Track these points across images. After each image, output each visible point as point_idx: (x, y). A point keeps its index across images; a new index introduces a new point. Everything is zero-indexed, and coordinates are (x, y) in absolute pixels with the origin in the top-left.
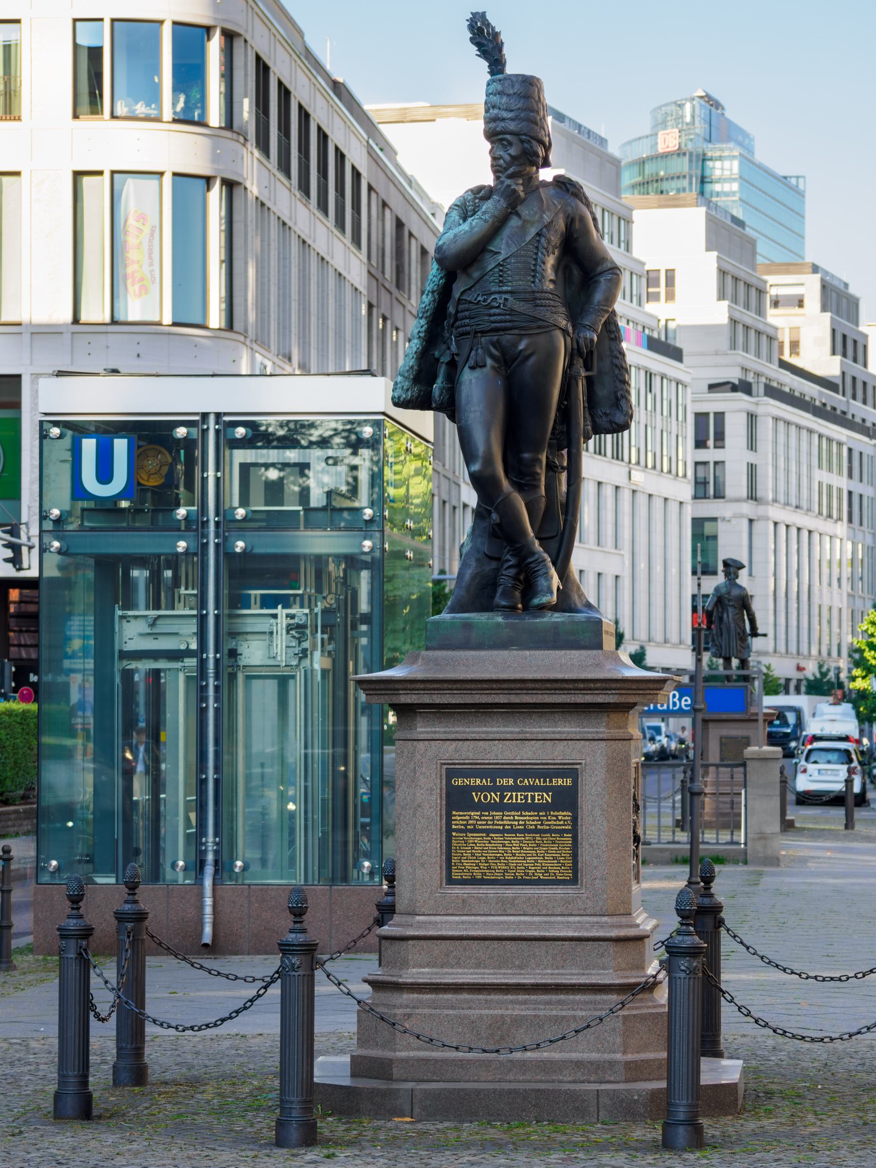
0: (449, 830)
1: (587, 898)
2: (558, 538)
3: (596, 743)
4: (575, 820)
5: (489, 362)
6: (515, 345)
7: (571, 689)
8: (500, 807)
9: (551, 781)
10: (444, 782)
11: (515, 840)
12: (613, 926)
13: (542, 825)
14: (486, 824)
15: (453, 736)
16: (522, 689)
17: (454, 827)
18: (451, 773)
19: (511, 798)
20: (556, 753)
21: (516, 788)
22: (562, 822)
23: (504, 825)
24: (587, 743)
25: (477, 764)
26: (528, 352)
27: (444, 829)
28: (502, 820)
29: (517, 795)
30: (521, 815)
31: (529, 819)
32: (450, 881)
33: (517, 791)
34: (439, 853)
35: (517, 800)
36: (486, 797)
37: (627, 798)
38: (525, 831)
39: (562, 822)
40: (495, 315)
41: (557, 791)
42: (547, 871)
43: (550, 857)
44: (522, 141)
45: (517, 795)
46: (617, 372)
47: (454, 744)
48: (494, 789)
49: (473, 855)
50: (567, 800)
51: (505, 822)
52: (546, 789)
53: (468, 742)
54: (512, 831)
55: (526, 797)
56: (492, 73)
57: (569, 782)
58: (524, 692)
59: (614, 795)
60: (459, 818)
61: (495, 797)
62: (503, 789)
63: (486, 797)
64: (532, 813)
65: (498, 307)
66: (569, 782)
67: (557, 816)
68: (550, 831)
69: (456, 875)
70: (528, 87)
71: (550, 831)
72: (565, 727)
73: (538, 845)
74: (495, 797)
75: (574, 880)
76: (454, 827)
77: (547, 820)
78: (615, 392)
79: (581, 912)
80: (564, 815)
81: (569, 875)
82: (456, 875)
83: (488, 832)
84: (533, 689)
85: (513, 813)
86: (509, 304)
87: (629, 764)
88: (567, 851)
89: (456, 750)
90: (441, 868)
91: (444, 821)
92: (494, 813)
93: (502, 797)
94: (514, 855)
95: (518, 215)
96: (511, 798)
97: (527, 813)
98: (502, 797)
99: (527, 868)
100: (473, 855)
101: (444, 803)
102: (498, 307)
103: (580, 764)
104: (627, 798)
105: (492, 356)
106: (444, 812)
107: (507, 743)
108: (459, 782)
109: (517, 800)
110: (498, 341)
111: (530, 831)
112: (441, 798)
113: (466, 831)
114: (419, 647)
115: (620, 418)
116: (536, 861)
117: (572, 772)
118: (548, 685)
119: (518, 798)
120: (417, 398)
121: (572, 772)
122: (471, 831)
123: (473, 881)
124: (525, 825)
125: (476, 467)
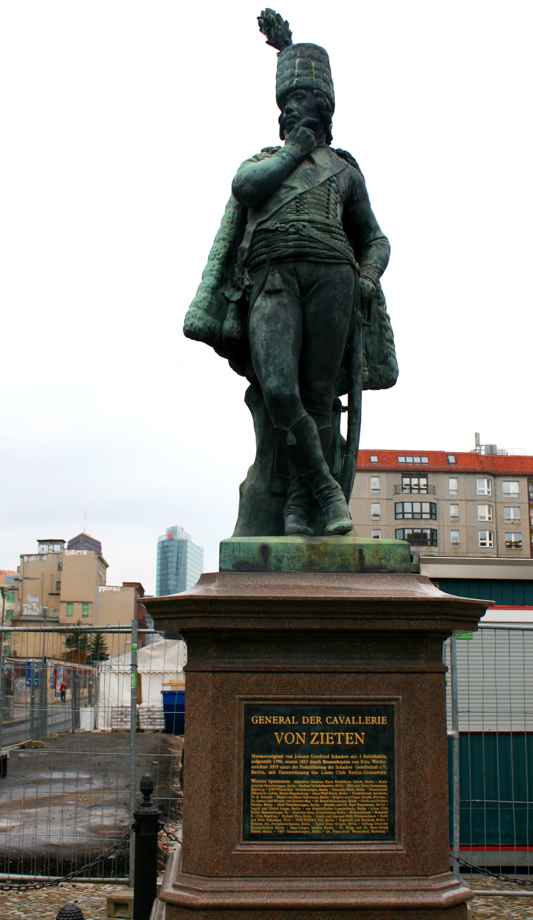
1: (407, 855)
9: (363, 720)
14: (291, 770)
17: (253, 772)
18: (251, 710)
19: (318, 738)
22: (376, 767)
23: (310, 771)
28: (309, 764)
29: (325, 736)
30: (330, 759)
31: (341, 762)
35: (325, 740)
39: (376, 767)
42: (359, 824)
45: (325, 736)
47: (255, 676)
49: (275, 805)
53: (270, 676)
55: (336, 738)
57: (383, 720)
60: (259, 761)
61: (300, 738)
62: (309, 728)
64: (342, 757)
66: (383, 720)
67: (370, 760)
74: (300, 738)
75: (390, 835)
77: (360, 765)
80: (378, 759)
81: (384, 828)
83: (292, 778)
84: (352, 613)
85: (321, 756)
93: (309, 738)
94: (322, 805)
96: (318, 738)
100: (275, 805)
103: (397, 700)
108: (259, 720)
109: (325, 740)
111: (340, 777)
124: (334, 770)
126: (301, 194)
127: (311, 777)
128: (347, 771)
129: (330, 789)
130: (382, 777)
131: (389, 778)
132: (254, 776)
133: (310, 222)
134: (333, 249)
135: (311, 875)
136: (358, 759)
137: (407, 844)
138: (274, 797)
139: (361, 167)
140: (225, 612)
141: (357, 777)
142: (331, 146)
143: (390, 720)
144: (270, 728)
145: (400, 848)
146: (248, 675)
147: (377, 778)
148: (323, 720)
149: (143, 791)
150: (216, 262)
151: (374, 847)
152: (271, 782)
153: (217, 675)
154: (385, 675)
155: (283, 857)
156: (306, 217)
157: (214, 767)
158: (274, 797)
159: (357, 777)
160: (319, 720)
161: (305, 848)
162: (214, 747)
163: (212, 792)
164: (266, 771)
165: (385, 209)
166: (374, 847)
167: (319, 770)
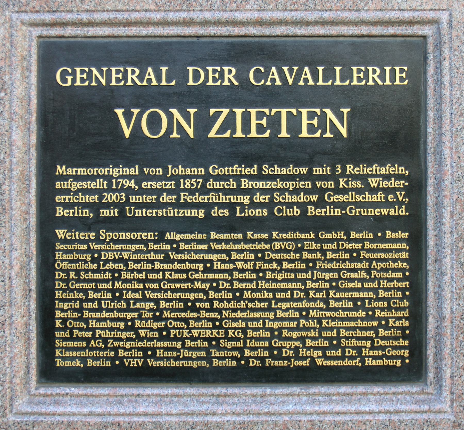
4: (416, 188)
8: (197, 151)
9: (347, 75)
11: (240, 249)
13: (320, 204)
14: (158, 205)
17: (60, 212)
18: (53, 54)
19: (230, 123)
22: (379, 197)
23: (208, 206)
28: (204, 191)
30: (260, 177)
31: (285, 189)
35: (393, 79)
36: (154, 122)
39: (379, 197)
41: (360, 101)
42: (335, 343)
48: (181, 97)
49: (117, 295)
51: (212, 197)
54: (231, 224)
55: (274, 122)
60: (79, 184)
61: (181, 122)
62: (204, 98)
63: (154, 122)
64: (292, 170)
66: (398, 76)
67: (364, 178)
73: (311, 266)
76: (60, 212)
77: (338, 191)
80: (386, 174)
83: (161, 226)
85: (235, 170)
88: (394, 281)
92: (181, 170)
93: (204, 124)
96: (230, 123)
97: (278, 170)
98: (204, 124)
99: (277, 334)
100: (117, 295)
108: (76, 77)
109: (393, 79)
111: (287, 224)
113: (96, 224)
116: (304, 313)
119: (249, 123)
124: (270, 205)
127: (209, 224)
128: (303, 206)
129: (259, 255)
136: (334, 177)
138: (116, 276)
143: (417, 75)
144: (108, 98)
147: (380, 224)
152: (105, 235)
167: (231, 206)
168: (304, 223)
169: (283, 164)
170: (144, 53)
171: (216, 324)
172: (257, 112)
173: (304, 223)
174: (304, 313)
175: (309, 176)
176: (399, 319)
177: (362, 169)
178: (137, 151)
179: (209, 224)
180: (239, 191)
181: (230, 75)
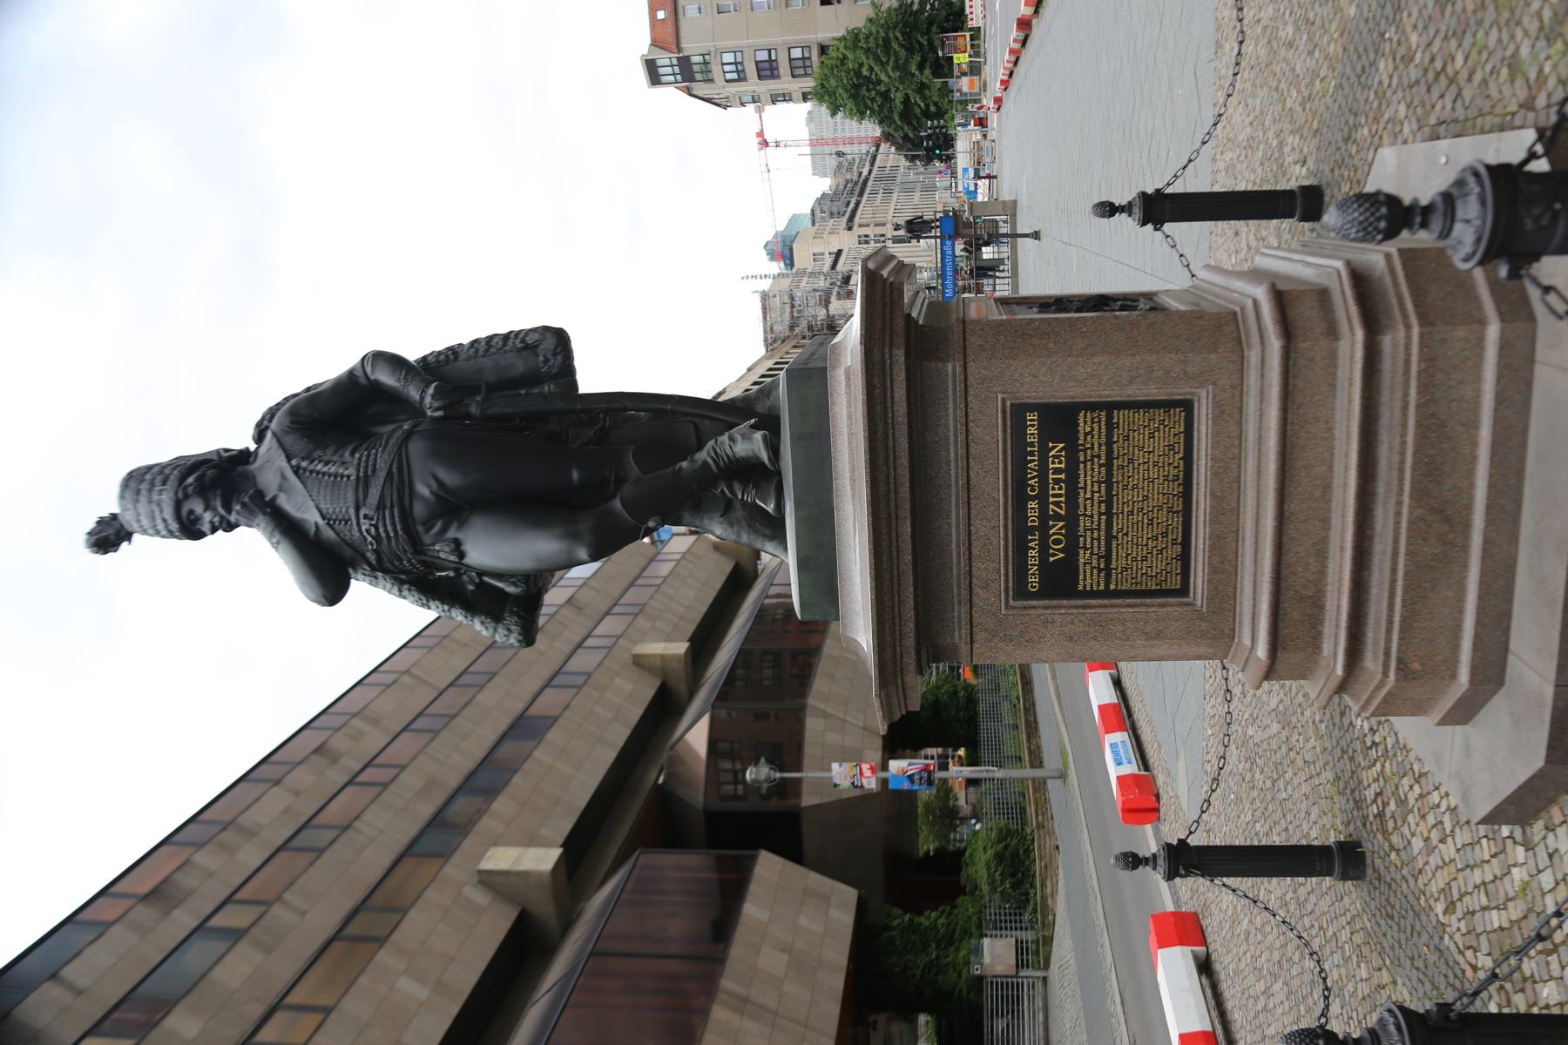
0: (1106, 594)
1: (1215, 384)
2: (697, 421)
3: (970, 378)
4: (1092, 407)
5: (451, 534)
6: (425, 500)
7: (886, 423)
8: (1071, 520)
9: (1032, 444)
10: (1034, 603)
11: (1123, 497)
12: (1394, 364)
13: (1099, 456)
14: (1099, 539)
15: (965, 593)
16: (889, 501)
17: (1102, 587)
18: (1021, 592)
19: (1057, 504)
20: (988, 438)
21: (1043, 499)
22: (1096, 426)
23: (1100, 514)
24: (971, 391)
25: (1006, 556)
26: (434, 485)
27: (1106, 602)
28: (1092, 516)
29: (1054, 496)
30: (1085, 488)
31: (1090, 477)
32: (1183, 591)
33: (1048, 496)
34: (1142, 609)
35: (1060, 496)
36: (1057, 542)
37: (1054, 324)
38: (1109, 482)
39: (1096, 426)
40: (386, 531)
41: (1045, 436)
42: (1171, 447)
43: (1147, 443)
44: (186, 497)
45: (1054, 496)
46: (493, 350)
47: (977, 590)
48: (1044, 528)
49: (1144, 559)
50: (1060, 420)
51: (1095, 512)
52: (1044, 451)
53: (974, 570)
54: (1109, 502)
55: (1057, 481)
56: (128, 536)
57: (1032, 417)
58: (892, 496)
59: (1051, 345)
60: (1088, 578)
61: (1057, 528)
62: (1044, 516)
63: (1057, 542)
64: (1081, 472)
65: (376, 527)
66: (1032, 417)
67: (1086, 434)
68: (1109, 443)
69: (1176, 583)
70: (138, 482)
71: (1109, 443)
72: (947, 426)
73: (1131, 461)
74: (1057, 528)
75: (1187, 406)
76: (1102, 587)
77: (1092, 448)
78: (519, 350)
79: (1237, 393)
80: (1084, 423)
81: (1178, 414)
82: (1176, 583)
83: (1110, 537)
84: (888, 483)
85: (1081, 500)
86: (371, 513)
87: (1002, 323)
88: (1140, 417)
89: (986, 587)
90: (1163, 606)
91: (1093, 602)
92: (1081, 528)
93: (1057, 517)
94: (1146, 498)
95: (274, 498)
96: (1057, 504)
97: (1082, 479)
98: (1057, 517)
99: (1166, 478)
100: (1144, 559)
101: (1065, 602)
102: (376, 527)
103: (1004, 401)
104: (1054, 324)
105: (444, 530)
106: (1080, 602)
107: (973, 512)
108: (1034, 581)
109: (1060, 496)
110: (424, 524)
111: (1109, 474)
112: (1059, 607)
113: (1108, 570)
114: (951, 102)
115: (549, 344)
116: (1156, 464)
117: (1018, 412)
118: (881, 461)
119: (1057, 493)
120: (519, 617)
121: (1018, 412)
122: (1108, 562)
123: (1185, 558)
124: (1100, 483)
125: (583, 554)
126: (323, 517)
127: (1109, 514)
128: (1101, 466)
129: (1125, 487)
130: (1109, 418)
131: (1110, 407)
132: (1107, 584)
133: (357, 509)
134: (389, 474)
135: (1237, 511)
136: (1085, 450)
137: (1201, 386)
138: (1134, 559)
139: (273, 403)
140: (894, 647)
141: (1109, 452)
142: (253, 447)
143: (1031, 407)
144: (1043, 564)
145: (1204, 394)
146: (975, 599)
147: (1110, 426)
148: (1033, 498)
149: (1112, 215)
150: (431, 604)
151: (1203, 428)
152: (1113, 565)
153: (976, 638)
154: (971, 417)
155: (1212, 548)
156: (352, 511)
157: (1095, 638)
158: (1134, 559)
159: (1109, 452)
160: (1032, 504)
161: (1201, 520)
162: (1070, 639)
163: (1127, 639)
164: (1100, 570)
165: (326, 362)
166: (1203, 428)
167: (1100, 502)
168: (1109, 465)
169: (1078, 476)
170: (1021, 549)
171: (1160, 509)
172: (799, 769)
173: (1109, 465)
174: (1156, 464)
175: (1085, 463)
176: (1159, 414)
177: (1082, 437)
178: (1072, 549)
179: (1109, 514)
180: (1092, 499)
181: (1032, 504)
